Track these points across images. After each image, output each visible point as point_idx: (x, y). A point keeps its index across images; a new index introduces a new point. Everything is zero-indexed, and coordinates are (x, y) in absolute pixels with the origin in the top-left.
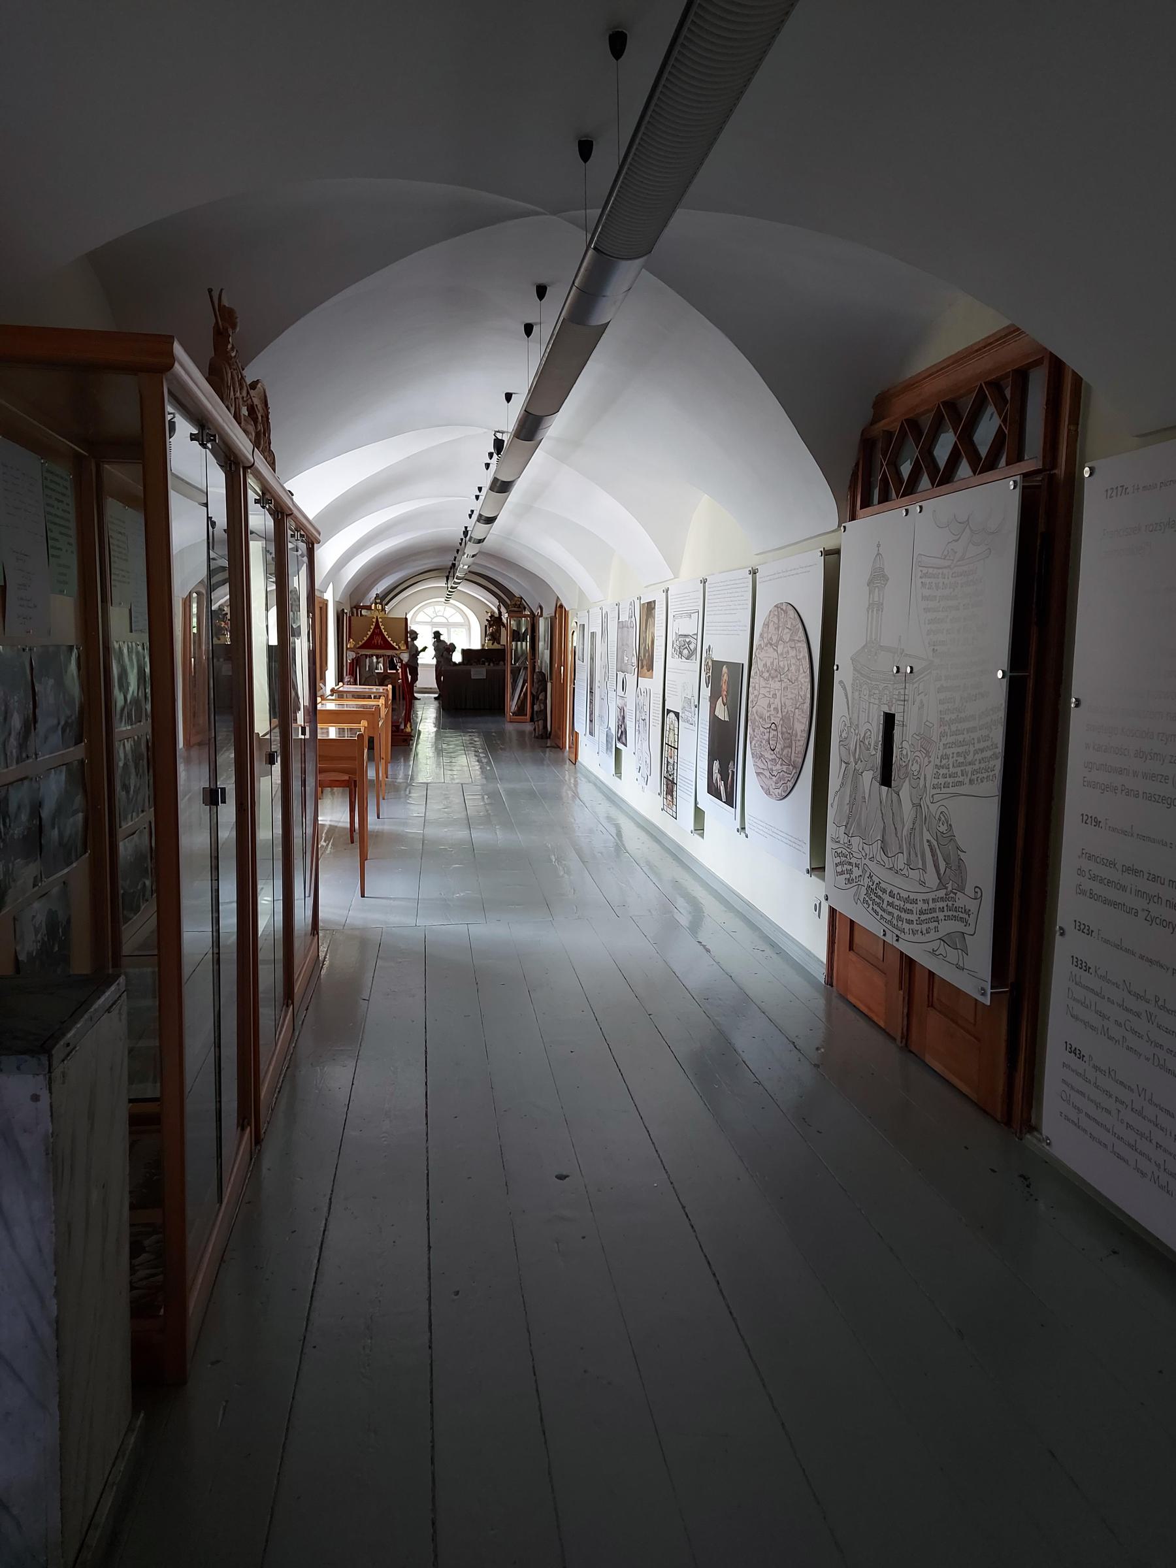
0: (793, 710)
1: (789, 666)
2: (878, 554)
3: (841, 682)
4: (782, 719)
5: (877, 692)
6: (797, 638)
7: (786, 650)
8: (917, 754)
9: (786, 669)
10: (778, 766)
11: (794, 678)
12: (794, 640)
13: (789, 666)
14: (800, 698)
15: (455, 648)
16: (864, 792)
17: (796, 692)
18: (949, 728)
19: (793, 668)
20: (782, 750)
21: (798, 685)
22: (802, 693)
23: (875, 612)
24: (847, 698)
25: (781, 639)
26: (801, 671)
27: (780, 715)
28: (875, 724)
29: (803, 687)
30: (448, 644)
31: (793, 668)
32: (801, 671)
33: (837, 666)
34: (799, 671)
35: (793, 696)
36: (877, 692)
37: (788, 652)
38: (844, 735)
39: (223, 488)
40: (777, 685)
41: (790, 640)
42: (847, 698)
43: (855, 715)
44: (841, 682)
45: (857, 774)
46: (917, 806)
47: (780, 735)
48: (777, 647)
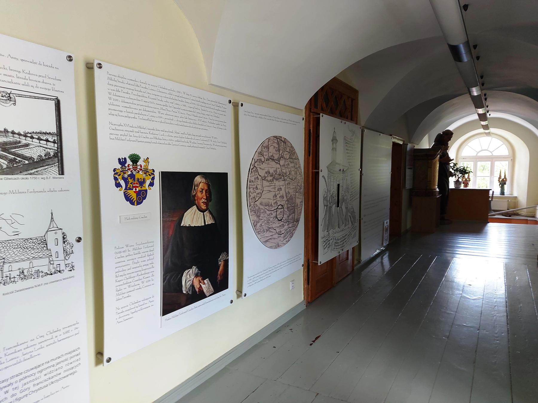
0: (295, 194)
1: (290, 172)
2: (334, 132)
3: (323, 176)
4: (287, 200)
5: (335, 178)
6: (294, 157)
7: (287, 163)
8: (346, 194)
9: (288, 173)
10: (286, 227)
11: (294, 178)
12: (292, 158)
13: (290, 172)
14: (298, 187)
15: (228, 288)
16: (333, 213)
17: (296, 184)
18: (204, 199)
19: (293, 173)
20: (288, 217)
21: (297, 181)
22: (300, 184)
23: (334, 151)
24: (326, 182)
25: (282, 157)
26: (298, 174)
27: (285, 199)
28: (335, 188)
29: (300, 181)
30: (129, 202)
31: (293, 173)
32: (298, 174)
33: (359, 170)
34: (297, 174)
35: (294, 187)
36: (335, 178)
37: (288, 164)
38: (325, 196)
39: (473, 187)
40: (282, 183)
41: (289, 158)
42: (326, 182)
43: (329, 188)
44: (323, 176)
45: (331, 207)
46: (347, 208)
47: (286, 210)
48: (279, 161)
